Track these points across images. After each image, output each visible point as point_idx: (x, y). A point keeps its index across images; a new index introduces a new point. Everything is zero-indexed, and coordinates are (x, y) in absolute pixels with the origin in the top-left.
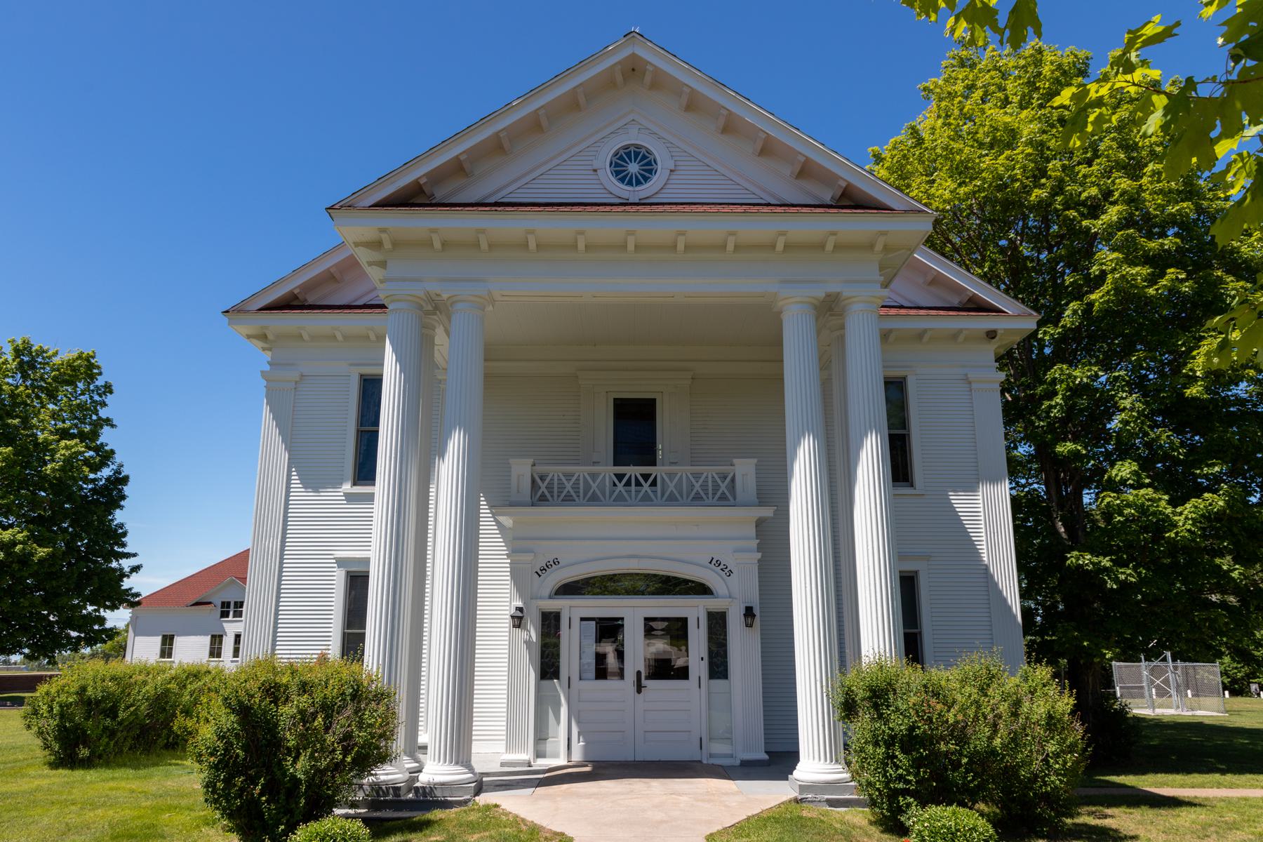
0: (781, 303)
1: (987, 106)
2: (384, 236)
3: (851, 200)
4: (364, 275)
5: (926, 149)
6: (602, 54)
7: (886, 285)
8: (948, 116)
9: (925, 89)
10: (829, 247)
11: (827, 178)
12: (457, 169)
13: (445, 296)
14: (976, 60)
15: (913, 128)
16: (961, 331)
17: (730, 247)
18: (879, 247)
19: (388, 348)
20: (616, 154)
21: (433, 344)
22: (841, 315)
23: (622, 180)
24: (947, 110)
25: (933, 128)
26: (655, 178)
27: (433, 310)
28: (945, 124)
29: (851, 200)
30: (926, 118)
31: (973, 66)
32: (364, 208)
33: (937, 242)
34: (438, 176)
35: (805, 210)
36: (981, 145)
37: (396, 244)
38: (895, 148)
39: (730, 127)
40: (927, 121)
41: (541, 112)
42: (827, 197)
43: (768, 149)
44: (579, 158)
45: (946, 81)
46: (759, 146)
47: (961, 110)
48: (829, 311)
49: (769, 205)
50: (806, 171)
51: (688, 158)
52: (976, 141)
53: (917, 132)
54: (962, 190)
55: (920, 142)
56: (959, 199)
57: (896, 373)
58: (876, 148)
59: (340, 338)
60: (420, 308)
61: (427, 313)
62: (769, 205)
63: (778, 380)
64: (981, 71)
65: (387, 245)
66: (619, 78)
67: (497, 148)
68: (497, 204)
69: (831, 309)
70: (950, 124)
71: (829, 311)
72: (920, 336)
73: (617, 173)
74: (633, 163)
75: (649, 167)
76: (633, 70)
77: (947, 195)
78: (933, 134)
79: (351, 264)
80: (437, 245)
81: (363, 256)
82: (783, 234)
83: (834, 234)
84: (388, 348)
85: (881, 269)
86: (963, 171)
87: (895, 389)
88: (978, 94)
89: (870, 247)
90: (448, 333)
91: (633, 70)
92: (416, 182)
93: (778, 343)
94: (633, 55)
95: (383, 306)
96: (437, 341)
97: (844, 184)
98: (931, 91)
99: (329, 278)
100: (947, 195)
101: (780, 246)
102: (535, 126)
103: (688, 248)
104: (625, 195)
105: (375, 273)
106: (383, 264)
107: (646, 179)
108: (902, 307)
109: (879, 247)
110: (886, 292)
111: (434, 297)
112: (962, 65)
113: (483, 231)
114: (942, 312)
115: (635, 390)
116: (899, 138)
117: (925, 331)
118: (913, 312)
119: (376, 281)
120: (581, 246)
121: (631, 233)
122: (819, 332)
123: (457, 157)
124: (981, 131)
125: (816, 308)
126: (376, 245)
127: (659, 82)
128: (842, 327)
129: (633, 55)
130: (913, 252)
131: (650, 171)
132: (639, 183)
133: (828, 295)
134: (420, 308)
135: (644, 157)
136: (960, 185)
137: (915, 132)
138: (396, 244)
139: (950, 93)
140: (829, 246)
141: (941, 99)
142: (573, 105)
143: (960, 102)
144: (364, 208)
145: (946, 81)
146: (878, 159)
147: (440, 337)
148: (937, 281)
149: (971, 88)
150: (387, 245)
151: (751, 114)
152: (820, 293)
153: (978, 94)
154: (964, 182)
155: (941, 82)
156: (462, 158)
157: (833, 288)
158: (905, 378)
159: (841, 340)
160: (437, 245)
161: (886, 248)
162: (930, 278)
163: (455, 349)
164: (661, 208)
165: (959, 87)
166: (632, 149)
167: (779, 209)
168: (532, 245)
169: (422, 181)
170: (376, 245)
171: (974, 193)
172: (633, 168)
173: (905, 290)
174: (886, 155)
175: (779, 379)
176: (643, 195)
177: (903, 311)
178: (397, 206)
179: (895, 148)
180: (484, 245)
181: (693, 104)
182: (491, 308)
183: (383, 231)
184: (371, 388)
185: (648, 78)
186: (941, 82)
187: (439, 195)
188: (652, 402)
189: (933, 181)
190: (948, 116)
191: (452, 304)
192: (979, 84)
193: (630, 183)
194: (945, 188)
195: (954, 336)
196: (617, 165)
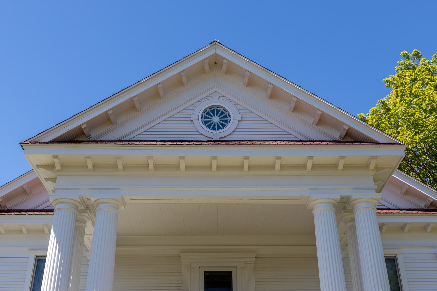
0: (312, 203)
1: (425, 89)
2: (56, 160)
3: (351, 138)
4: (44, 190)
5: (392, 115)
6: (197, 52)
7: (379, 191)
8: (403, 95)
9: (387, 82)
10: (341, 166)
11: (335, 124)
12: (106, 120)
13: (93, 200)
14: (415, 66)
15: (383, 102)
16: (428, 224)
17: (278, 167)
18: (372, 167)
19: (52, 235)
20: (205, 111)
21: (84, 232)
22: (352, 211)
23: (209, 127)
24: (402, 91)
25: (395, 103)
26: (229, 125)
27: (86, 208)
28: (401, 101)
29: (351, 138)
30: (389, 98)
31: (414, 69)
32: (45, 143)
33: (405, 166)
34: (94, 124)
35: (323, 143)
36: (425, 111)
37: (64, 166)
38: (373, 114)
39: (274, 95)
40: (391, 99)
41: (159, 86)
42: (337, 136)
43: (298, 108)
44: (184, 113)
45: (399, 76)
46: (293, 106)
47: (411, 91)
48: (344, 208)
49: (301, 141)
50: (322, 120)
51: (248, 112)
52: (422, 108)
53: (385, 105)
54: (417, 137)
55: (388, 110)
56: (416, 143)
57: (391, 253)
58: (362, 114)
59: (24, 231)
60: (76, 207)
61: (81, 212)
62: (301, 141)
63: (313, 258)
64: (419, 71)
65: (58, 167)
66: (207, 68)
67: (132, 107)
68: (130, 141)
69: (344, 208)
70: (405, 100)
71: (344, 208)
72: (402, 228)
73: (206, 122)
74: (216, 117)
75: (225, 119)
76: (216, 63)
77: (408, 140)
78: (395, 106)
79: (36, 184)
80: (90, 166)
81: (42, 174)
82: (311, 158)
83: (343, 158)
84: (52, 235)
85: (375, 181)
86: (416, 126)
87: (391, 262)
88: (419, 83)
89: (367, 167)
90: (93, 224)
91: (216, 63)
92: (80, 127)
93: (312, 233)
94: (216, 53)
95: (52, 210)
96: (87, 231)
97: (347, 128)
98: (391, 82)
99: (23, 192)
100: (408, 140)
101: (309, 167)
102: (155, 95)
103: (251, 168)
104: (210, 135)
105: (49, 186)
106: (54, 180)
107: (224, 126)
108: (388, 209)
109: (372, 167)
110: (379, 196)
111: (86, 201)
112: (407, 68)
113: (119, 157)
114: (415, 212)
115: (218, 265)
116: (376, 108)
117: (405, 224)
118: (396, 212)
119: (51, 193)
120: (182, 167)
121: (215, 158)
122: (338, 223)
123: (106, 112)
124: (423, 103)
125: (335, 206)
126: (51, 167)
127: (231, 70)
128: (353, 220)
129: (216, 54)
130: (392, 173)
131: (226, 121)
132: (219, 128)
133: (342, 198)
134: (76, 207)
135: (223, 113)
136: (415, 134)
137: (384, 105)
138: (64, 166)
139: (402, 83)
140: (341, 166)
141: (397, 87)
142: (179, 82)
143: (409, 87)
144: (45, 143)
145: (399, 76)
146: (363, 119)
147: (89, 229)
148: (409, 192)
149: (414, 81)
150: (58, 167)
151: (286, 87)
152: (337, 196)
153: (419, 83)
154: (418, 132)
155: (396, 77)
156: (109, 113)
157: (346, 193)
158: (395, 256)
159: (353, 228)
160: (90, 166)
161: (377, 168)
162: (404, 190)
163: (98, 237)
164: (233, 143)
165: (407, 80)
166: (215, 108)
167: (307, 143)
168: (151, 166)
169: (83, 127)
170: (51, 167)
171: (425, 139)
172: (216, 119)
173: (392, 198)
174: (369, 118)
175: (315, 257)
176: (222, 135)
177: (389, 212)
178: (66, 142)
179: (373, 114)
180: (120, 167)
181: (252, 82)
182: (122, 208)
183: (55, 157)
184: (40, 263)
185: (224, 67)
186: (396, 77)
187: (94, 135)
188: (229, 275)
189: (399, 133)
190: (403, 95)
191: (98, 204)
192: (419, 78)
193: (214, 128)
194: (407, 136)
195: (425, 228)
196: (206, 118)
